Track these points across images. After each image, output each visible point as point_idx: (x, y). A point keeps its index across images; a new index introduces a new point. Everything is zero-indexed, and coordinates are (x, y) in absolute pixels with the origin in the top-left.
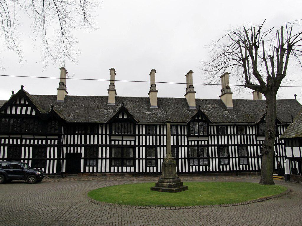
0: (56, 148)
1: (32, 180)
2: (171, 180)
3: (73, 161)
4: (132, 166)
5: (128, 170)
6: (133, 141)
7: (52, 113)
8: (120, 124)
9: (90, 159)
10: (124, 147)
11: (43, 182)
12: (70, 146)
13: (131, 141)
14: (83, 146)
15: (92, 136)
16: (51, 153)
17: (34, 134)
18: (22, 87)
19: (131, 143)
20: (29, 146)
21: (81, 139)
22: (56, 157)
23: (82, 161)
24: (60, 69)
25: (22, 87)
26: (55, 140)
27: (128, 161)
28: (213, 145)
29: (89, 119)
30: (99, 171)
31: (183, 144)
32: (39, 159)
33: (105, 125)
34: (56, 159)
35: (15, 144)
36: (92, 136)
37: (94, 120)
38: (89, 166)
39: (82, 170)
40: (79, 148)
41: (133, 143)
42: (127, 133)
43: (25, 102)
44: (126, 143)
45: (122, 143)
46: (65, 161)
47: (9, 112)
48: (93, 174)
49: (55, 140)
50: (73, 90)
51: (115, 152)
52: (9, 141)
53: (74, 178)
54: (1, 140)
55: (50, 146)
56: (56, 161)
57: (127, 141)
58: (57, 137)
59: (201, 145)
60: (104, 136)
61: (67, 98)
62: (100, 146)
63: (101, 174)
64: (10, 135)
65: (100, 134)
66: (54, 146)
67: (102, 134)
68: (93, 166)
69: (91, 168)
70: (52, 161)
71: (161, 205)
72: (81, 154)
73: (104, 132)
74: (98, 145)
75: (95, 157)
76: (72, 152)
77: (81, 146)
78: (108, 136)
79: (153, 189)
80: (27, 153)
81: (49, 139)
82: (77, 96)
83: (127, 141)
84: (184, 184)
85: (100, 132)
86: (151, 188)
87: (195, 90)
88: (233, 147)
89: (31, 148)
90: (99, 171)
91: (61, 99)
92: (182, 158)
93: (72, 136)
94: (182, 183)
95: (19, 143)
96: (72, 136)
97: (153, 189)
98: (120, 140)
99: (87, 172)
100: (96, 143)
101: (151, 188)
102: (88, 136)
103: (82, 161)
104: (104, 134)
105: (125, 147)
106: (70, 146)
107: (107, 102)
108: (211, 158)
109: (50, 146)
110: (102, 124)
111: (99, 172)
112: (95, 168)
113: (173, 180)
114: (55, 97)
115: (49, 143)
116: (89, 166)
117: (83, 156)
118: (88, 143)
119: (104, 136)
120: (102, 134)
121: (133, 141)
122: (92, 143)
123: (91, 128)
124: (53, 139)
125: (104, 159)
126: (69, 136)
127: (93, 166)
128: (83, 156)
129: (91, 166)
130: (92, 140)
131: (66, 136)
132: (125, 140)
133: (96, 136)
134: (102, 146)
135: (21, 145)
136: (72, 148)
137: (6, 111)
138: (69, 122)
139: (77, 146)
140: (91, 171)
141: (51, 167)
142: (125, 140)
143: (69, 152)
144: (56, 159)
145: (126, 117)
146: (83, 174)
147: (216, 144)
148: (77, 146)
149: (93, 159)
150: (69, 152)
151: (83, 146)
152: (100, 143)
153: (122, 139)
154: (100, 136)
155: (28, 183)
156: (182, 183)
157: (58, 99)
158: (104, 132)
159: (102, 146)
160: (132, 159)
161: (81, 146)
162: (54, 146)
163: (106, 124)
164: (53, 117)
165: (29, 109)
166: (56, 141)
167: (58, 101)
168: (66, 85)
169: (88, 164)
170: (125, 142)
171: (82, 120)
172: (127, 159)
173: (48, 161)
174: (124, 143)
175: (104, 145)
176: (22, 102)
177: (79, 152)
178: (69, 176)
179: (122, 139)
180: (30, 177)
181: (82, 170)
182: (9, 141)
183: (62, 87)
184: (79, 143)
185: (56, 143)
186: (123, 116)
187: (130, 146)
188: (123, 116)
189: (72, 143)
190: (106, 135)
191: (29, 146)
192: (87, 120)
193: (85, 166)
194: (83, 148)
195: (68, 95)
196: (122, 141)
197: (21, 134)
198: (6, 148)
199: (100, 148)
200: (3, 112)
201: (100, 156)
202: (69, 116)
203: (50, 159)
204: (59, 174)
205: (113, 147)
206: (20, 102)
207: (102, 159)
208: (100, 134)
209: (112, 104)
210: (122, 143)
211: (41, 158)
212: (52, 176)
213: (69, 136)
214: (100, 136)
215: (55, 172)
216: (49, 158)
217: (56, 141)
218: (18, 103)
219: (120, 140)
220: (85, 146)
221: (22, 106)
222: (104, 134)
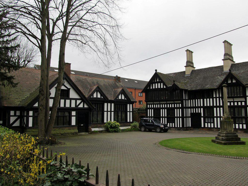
0: (180, 110)
1: (158, 130)
2: (224, 134)
3: (196, 118)
4: (244, 124)
5: (241, 127)
6: (243, 101)
7: (174, 85)
8: (232, 88)
9: (208, 117)
10: (236, 107)
11: (168, 132)
12: (193, 108)
13: (241, 102)
14: (202, 107)
15: (208, 99)
16: (178, 113)
17: (166, 101)
18: (156, 70)
19: (241, 104)
20: (165, 108)
21: (200, 102)
22: (181, 116)
23: (202, 119)
24: (186, 51)
25: (156, 70)
26: (179, 104)
27: (240, 119)
28: (218, 107)
29: (204, 87)
30: (216, 127)
31: (218, 105)
32: (171, 118)
33: (218, 90)
34: (181, 117)
35: (243, 105)
36: (208, 99)
37: (208, 87)
38: (208, 123)
39: (203, 126)
40: (199, 109)
41: (243, 104)
42: (237, 95)
43: (159, 80)
44: (238, 104)
45: (234, 104)
46: (190, 118)
47: (151, 88)
48: (210, 129)
49: (179, 104)
50: (198, 66)
51: (242, 112)
52: (167, 106)
53: (196, 131)
54: (10, 112)
55: (177, 108)
56: (181, 119)
57: (238, 102)
58: (180, 102)
59: (238, 106)
60: (218, 99)
61: (194, 72)
62: (215, 107)
63: (217, 129)
64: (234, 98)
65: (215, 98)
66: (179, 108)
67: (216, 98)
68: (211, 123)
69: (209, 124)
70: (164, 118)
71: (220, 154)
72: (201, 113)
73: (218, 96)
74: (213, 107)
75: (212, 116)
76: (194, 112)
77: (200, 107)
78: (221, 98)
79: (213, 141)
80: (163, 113)
81: (155, 104)
82: (201, 69)
83: (238, 102)
84: (241, 140)
85: (214, 96)
86: (212, 140)
87: (223, 61)
88: (218, 109)
89: (153, 110)
90: (216, 127)
91: (188, 73)
92: (165, 117)
93: (194, 100)
94: (240, 138)
95: (173, 106)
96: (194, 100)
97: (213, 141)
98: (232, 102)
99: (206, 128)
100: (211, 105)
101: (212, 140)
102: (205, 100)
103: (202, 119)
104: (218, 97)
105: (237, 107)
106: (193, 108)
107: (223, 71)
108: (215, 117)
109: (177, 108)
110: (215, 90)
111: (216, 128)
112: (212, 124)
113: (226, 135)
114: (184, 72)
115: (161, 107)
116: (208, 123)
117: (202, 115)
118: (205, 105)
119: (218, 99)
120: (216, 98)
121: (243, 101)
122: (208, 105)
123: (207, 93)
124: (164, 104)
125: (219, 117)
126: (192, 100)
127: (211, 123)
128: (202, 115)
129: (209, 123)
130: (208, 102)
131: (189, 101)
132: (236, 102)
133: (211, 99)
134: (217, 107)
135: (175, 108)
136: (194, 109)
137: (150, 87)
138: (189, 90)
139: (198, 107)
140: (209, 126)
141: (178, 123)
142: (236, 102)
143: (192, 112)
144: (181, 117)
145: (234, 81)
146: (204, 129)
147: (202, 105)
148: (198, 107)
149: (210, 118)
150: (192, 112)
151: (202, 107)
152: (215, 105)
153: (234, 100)
154: (215, 99)
155: (156, 132)
156: (240, 138)
157: (186, 74)
158: (218, 96)
159: (217, 107)
160: (243, 117)
161: (200, 107)
162: (179, 108)
163: (217, 89)
164: (175, 88)
165: (162, 84)
166: (180, 105)
167: (187, 75)
168: (233, 56)
169: (207, 121)
170: (233, 103)
171: (199, 88)
172: (239, 118)
173: (176, 119)
174: (236, 104)
175: (215, 106)
176: (158, 81)
177: (199, 112)
178: (193, 129)
179: (234, 100)
180: (157, 128)
181: (203, 126)
182: (167, 106)
183: (190, 63)
184: (199, 105)
185: (180, 106)
186: (232, 81)
187: (242, 106)
188: (232, 81)
189: (194, 106)
190: (219, 97)
191: (165, 108)
192: (202, 87)
193: (205, 122)
194: (202, 109)
195: (195, 69)
196: (234, 102)
197: (160, 101)
198: (166, 110)
199: (215, 109)
200: (148, 88)
201: (215, 115)
202: (191, 86)
203: (163, 117)
204: (184, 128)
205: (240, 107)
206: (157, 80)
207: (217, 117)
208: (215, 98)
209: (227, 71)
210: (234, 104)
211: (172, 117)
212: (179, 129)
213: (192, 100)
214: (215, 99)
215: (181, 126)
216: (219, 116)
217: (180, 105)
218: (155, 81)
219: (232, 102)
220: (204, 107)
221: (158, 83)
222: (218, 97)
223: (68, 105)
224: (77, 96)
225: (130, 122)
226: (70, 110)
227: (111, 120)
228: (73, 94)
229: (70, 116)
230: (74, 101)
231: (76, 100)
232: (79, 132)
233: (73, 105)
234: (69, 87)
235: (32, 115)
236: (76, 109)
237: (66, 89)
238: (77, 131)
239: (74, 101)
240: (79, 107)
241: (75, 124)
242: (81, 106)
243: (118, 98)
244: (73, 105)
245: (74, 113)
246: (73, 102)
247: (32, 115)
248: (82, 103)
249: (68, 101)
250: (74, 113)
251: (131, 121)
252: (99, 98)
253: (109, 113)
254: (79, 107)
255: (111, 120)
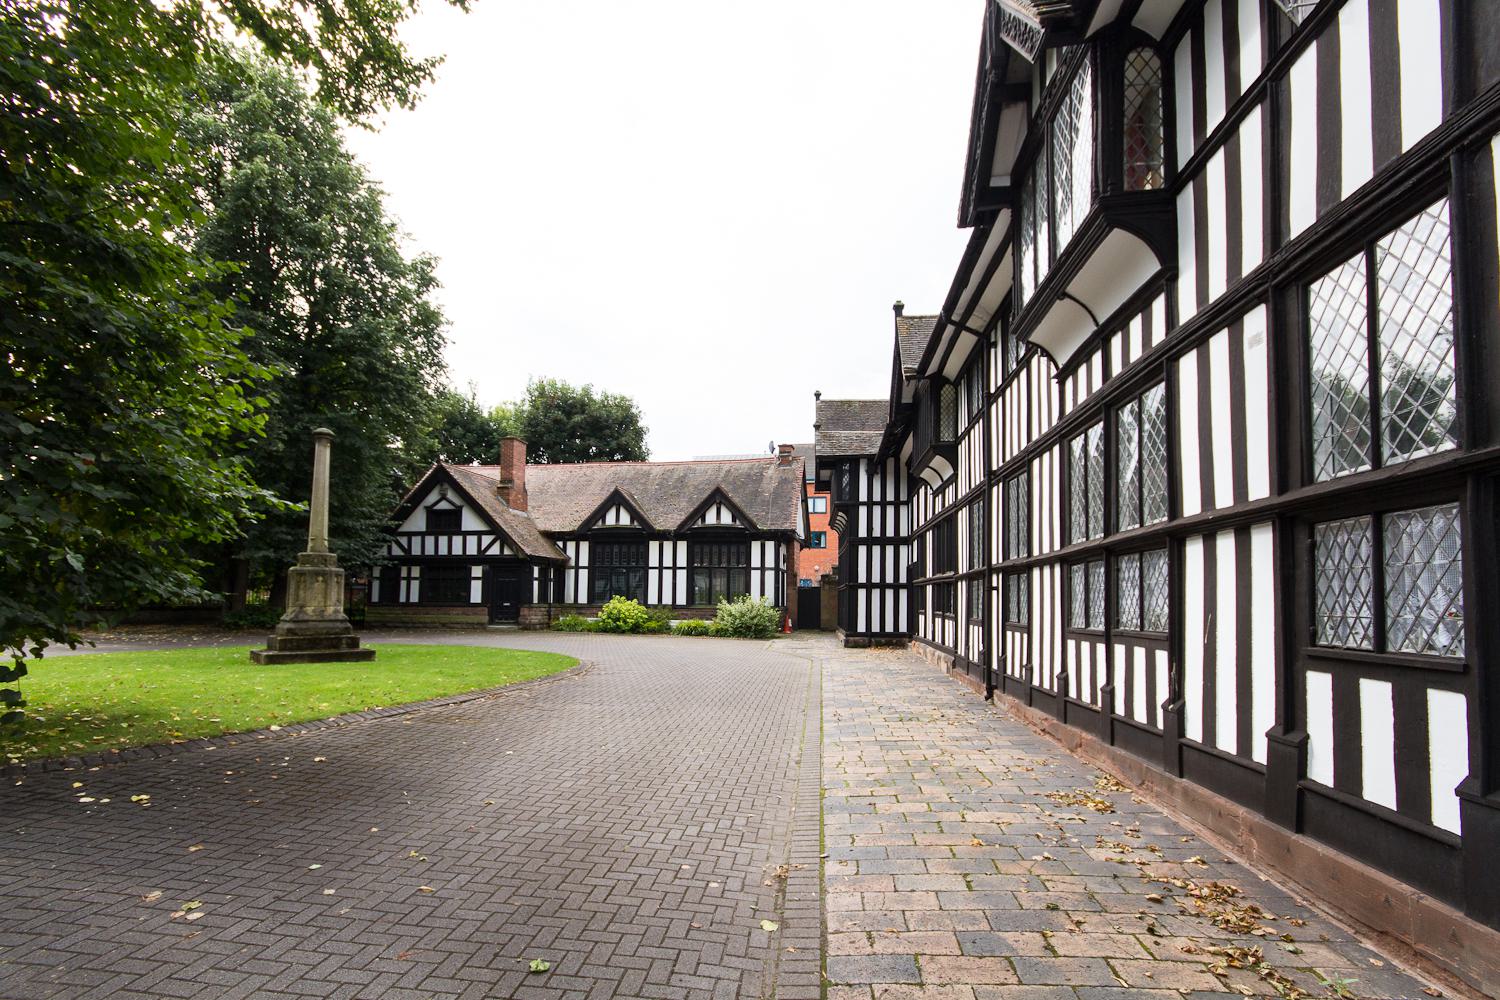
88: (876, 550)
92: (896, 587)
104: (890, 503)
108: (862, 586)
158: (890, 497)
203: (896, 587)
222: (890, 503)
223: (457, 550)
224: (480, 526)
225: (408, 604)
226: (467, 561)
227: (762, 593)
228: (469, 521)
229: (469, 579)
230: (419, 538)
231: (479, 534)
232: (491, 622)
233: (472, 550)
234: (458, 501)
235: (418, 575)
236: (481, 558)
237: (452, 507)
238: (485, 619)
239: (419, 538)
240: (489, 553)
241: (417, 600)
242: (495, 550)
243: (704, 520)
244: (472, 550)
245: (477, 571)
246: (472, 541)
247: (418, 575)
248: (497, 545)
249: (457, 540)
250: (477, 571)
251: (411, 600)
252: (624, 528)
253: (668, 575)
254: (489, 553)
255: (762, 593)
